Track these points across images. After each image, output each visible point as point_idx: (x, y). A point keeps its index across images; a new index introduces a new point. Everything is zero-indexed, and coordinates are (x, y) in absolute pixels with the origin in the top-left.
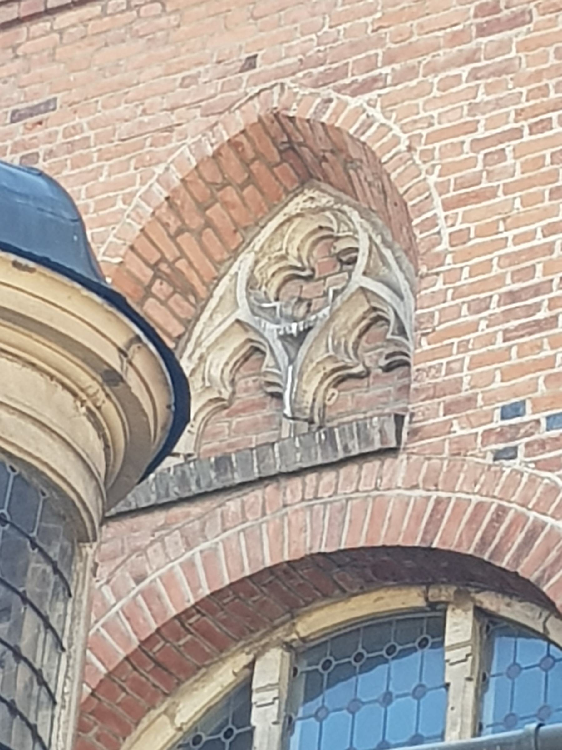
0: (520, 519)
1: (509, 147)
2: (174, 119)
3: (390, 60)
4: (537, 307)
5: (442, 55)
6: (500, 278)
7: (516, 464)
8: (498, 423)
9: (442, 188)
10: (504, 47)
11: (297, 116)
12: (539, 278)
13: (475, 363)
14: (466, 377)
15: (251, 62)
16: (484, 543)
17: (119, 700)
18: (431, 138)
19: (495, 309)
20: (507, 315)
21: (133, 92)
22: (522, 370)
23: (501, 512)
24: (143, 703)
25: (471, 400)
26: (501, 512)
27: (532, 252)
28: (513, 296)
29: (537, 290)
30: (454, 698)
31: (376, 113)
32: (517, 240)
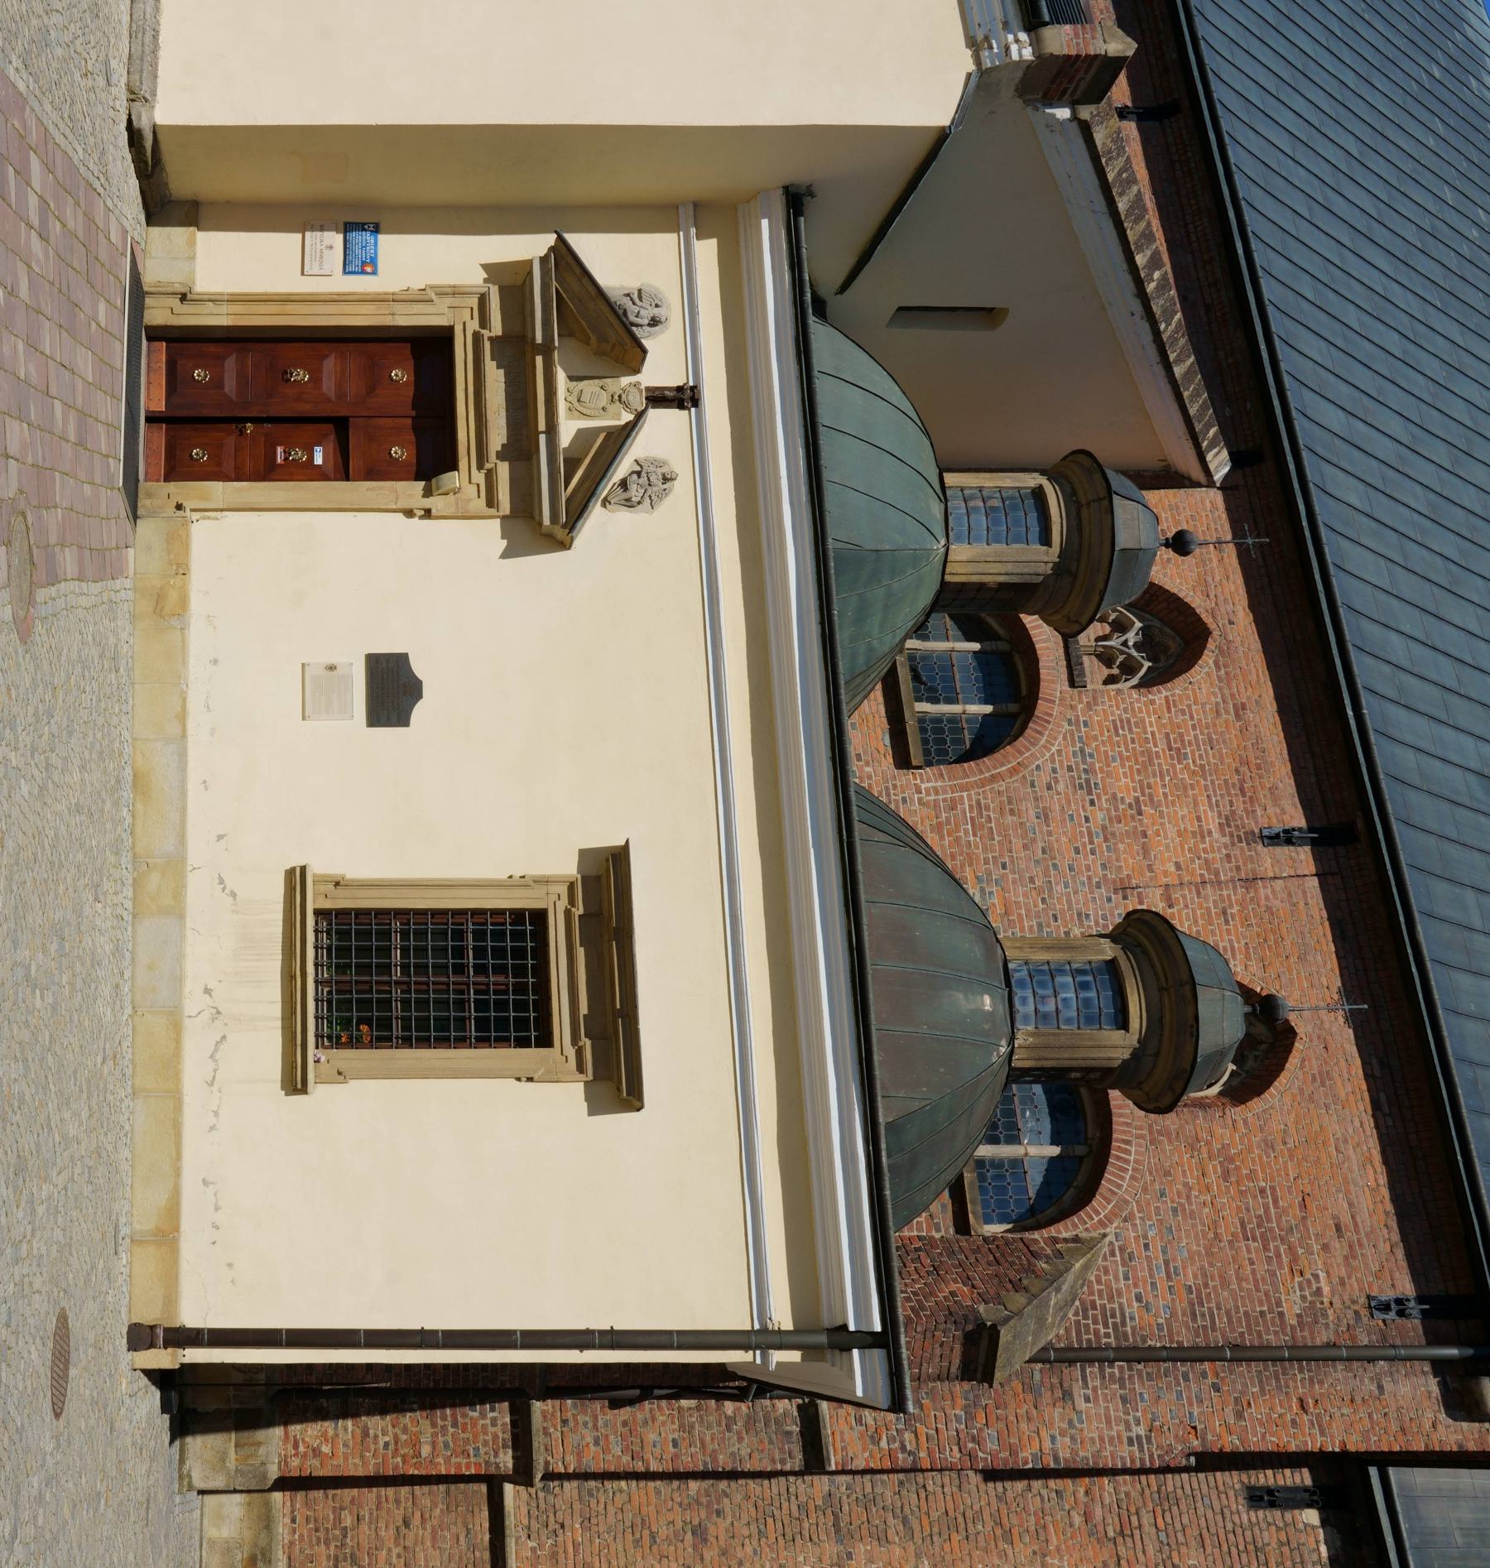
0: (1045, 728)
1: (1187, 717)
2: (1212, 597)
3: (1226, 673)
4: (1123, 730)
5: (1227, 692)
6: (1136, 717)
7: (1066, 726)
8: (1082, 719)
9: (1173, 695)
10: (1227, 712)
11: (162, 484)
12: (1135, 730)
13: (1104, 710)
14: (1099, 708)
15: (1231, 623)
16: (1038, 717)
17: (1122, 79)
18: (1194, 691)
19: (1124, 716)
20: (1121, 721)
21: (1224, 581)
22: (1100, 726)
23: (1048, 722)
24: (397, 925)
25: (1091, 710)
26: (1048, 722)
27: (1145, 728)
28: (1129, 721)
29: (1130, 730)
30: (972, 1202)
31: (1206, 669)
32: (1150, 722)
